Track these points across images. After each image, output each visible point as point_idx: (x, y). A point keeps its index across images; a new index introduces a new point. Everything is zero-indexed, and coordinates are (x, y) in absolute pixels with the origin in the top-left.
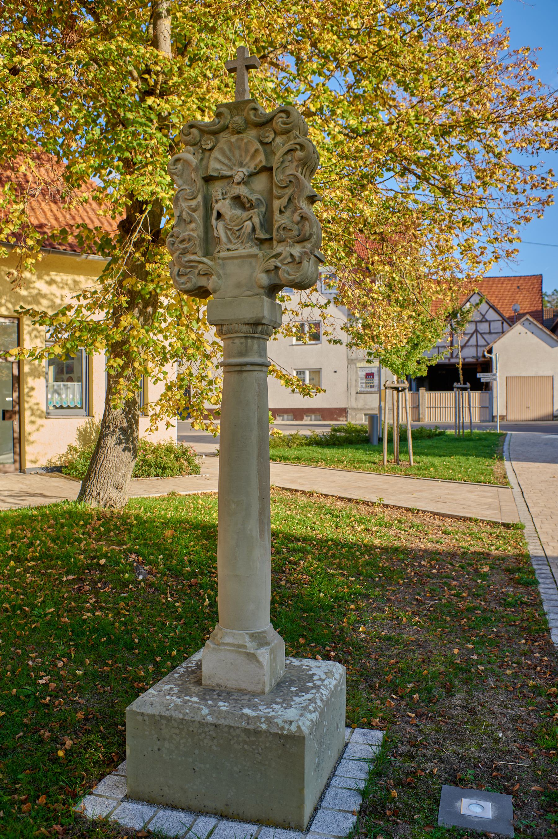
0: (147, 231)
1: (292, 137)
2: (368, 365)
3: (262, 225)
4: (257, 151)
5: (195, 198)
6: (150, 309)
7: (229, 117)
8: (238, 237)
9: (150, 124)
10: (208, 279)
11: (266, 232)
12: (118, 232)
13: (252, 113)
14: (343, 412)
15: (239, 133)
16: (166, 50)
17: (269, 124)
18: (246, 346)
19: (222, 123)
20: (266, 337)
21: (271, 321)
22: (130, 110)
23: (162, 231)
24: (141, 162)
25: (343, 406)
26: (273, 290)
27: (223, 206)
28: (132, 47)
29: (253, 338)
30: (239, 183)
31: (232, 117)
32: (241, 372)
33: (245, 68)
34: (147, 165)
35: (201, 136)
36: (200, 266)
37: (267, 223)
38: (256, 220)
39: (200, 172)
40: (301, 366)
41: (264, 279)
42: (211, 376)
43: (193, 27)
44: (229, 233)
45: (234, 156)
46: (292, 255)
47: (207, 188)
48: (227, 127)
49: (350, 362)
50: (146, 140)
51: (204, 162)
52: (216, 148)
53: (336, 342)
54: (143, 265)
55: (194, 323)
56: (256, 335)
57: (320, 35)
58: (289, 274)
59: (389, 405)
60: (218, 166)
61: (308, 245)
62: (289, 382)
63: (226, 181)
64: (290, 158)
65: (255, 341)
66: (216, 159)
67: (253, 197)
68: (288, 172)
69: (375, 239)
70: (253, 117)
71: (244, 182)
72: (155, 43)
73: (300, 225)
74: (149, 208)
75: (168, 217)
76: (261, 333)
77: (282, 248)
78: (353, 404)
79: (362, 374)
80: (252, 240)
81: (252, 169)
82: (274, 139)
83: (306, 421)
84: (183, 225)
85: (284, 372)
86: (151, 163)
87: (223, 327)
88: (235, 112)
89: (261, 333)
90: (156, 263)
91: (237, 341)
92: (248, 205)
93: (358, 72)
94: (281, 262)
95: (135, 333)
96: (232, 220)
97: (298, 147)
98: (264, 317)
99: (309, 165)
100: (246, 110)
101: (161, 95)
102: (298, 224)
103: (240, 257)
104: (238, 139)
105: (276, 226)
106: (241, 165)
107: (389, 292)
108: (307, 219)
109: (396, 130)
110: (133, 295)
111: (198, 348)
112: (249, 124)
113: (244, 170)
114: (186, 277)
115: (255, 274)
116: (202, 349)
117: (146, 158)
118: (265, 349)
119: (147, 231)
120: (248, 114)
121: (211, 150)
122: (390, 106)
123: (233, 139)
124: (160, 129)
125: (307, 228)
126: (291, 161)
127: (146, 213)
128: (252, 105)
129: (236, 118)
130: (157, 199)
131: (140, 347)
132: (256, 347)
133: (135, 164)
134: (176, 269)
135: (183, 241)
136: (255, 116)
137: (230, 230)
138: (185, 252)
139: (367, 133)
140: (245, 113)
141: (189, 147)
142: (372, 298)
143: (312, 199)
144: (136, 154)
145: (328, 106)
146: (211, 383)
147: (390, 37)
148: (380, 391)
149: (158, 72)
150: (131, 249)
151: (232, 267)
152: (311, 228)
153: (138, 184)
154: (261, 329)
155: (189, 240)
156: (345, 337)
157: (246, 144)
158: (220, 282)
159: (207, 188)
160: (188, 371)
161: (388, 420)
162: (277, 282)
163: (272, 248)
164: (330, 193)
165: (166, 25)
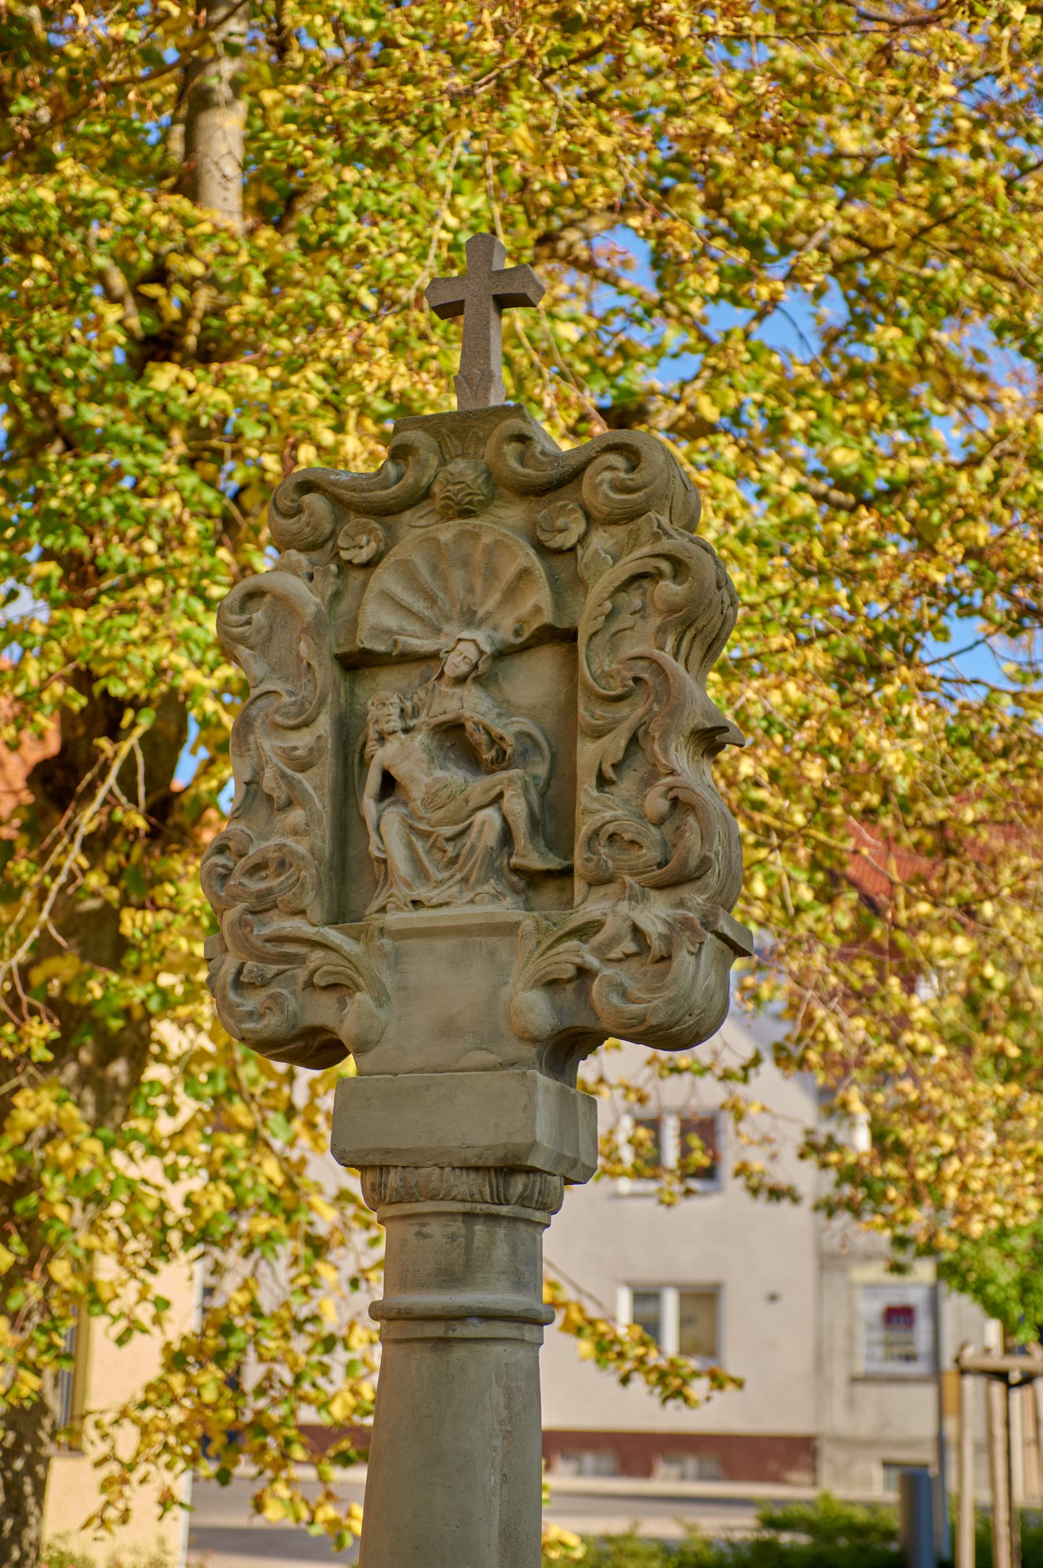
0: (133, 800)
1: (645, 535)
2: (894, 1278)
3: (535, 824)
4: (524, 573)
5: (306, 724)
6: (119, 1069)
7: (434, 462)
8: (453, 861)
9: (160, 445)
10: (342, 1004)
11: (551, 846)
12: (27, 798)
13: (511, 450)
14: (798, 1452)
15: (466, 513)
16: (224, 205)
17: (569, 488)
18: (468, 1248)
19: (409, 479)
20: (538, 1216)
21: (560, 1158)
22: (96, 396)
23: (186, 800)
24: (122, 568)
25: (799, 1425)
26: (568, 1047)
27: (406, 754)
28: (111, 194)
29: (495, 1218)
30: (460, 681)
31: (444, 462)
32: (446, 1341)
33: (491, 305)
34: (142, 578)
35: (339, 522)
36: (317, 956)
37: (554, 818)
38: (516, 806)
39: (330, 638)
40: (647, 1273)
41: (538, 1011)
42: (332, 1321)
43: (318, 153)
44: (419, 845)
45: (446, 589)
46: (636, 931)
47: (352, 693)
48: (427, 494)
49: (830, 1262)
50: (144, 495)
51: (345, 605)
52: (387, 562)
53: (776, 1194)
54: (109, 915)
55: (276, 1120)
56: (504, 1210)
57: (740, 173)
58: (625, 995)
59: (973, 1433)
60: (391, 620)
61: (696, 898)
62: (606, 1348)
63: (416, 671)
64: (637, 603)
65: (501, 1232)
66: (387, 596)
67: (508, 729)
68: (631, 648)
69: (918, 845)
70: (514, 464)
71: (478, 676)
72: (189, 185)
73: (668, 827)
74: (146, 721)
75: (204, 753)
76: (524, 1200)
77: (606, 905)
78: (838, 1420)
79: (872, 1308)
80: (498, 873)
81: (506, 634)
82: (582, 539)
83: (665, 1480)
84: (263, 812)
85: (593, 1312)
86: (160, 573)
87: (386, 1178)
88: (453, 444)
89: (524, 1200)
90: (158, 909)
91: (435, 1229)
92: (488, 755)
93: (862, 289)
94: (600, 951)
95: (64, 1152)
96: (431, 801)
97: (665, 566)
98: (533, 1145)
99: (702, 624)
100: (492, 442)
101: (204, 356)
102: (659, 823)
103: (459, 931)
104: (461, 535)
105: (584, 828)
106: (470, 618)
107: (969, 1026)
108: (691, 808)
109: (993, 489)
110: (72, 1017)
111: (289, 1215)
112: (498, 486)
113: (480, 636)
114: (264, 993)
115: (506, 991)
116: (302, 1217)
117: (142, 554)
118: (535, 1259)
119: (133, 800)
120: (499, 454)
121: (369, 565)
122: (969, 400)
123: (447, 532)
124: (191, 462)
125: (692, 839)
126: (641, 612)
127: (132, 741)
128: (513, 424)
129: (458, 466)
130: (173, 691)
131: (77, 1203)
132: (501, 1252)
133: (101, 573)
134: (229, 965)
135: (256, 869)
136: (522, 460)
137: (425, 835)
138: (263, 905)
139: (894, 491)
140: (488, 451)
141: (294, 554)
142: (912, 1048)
143: (710, 740)
144: (107, 543)
145: (760, 405)
146: (329, 1343)
147: (969, 182)
148: (937, 1375)
149: (194, 278)
150: (76, 858)
151: (427, 966)
152: (705, 837)
153: (111, 639)
154: (517, 1186)
155: (282, 864)
156: (810, 1180)
157: (490, 551)
158: (383, 1014)
159: (352, 693)
160: (243, 1298)
161: (969, 1488)
162: (583, 1020)
163: (569, 904)
164: (763, 693)
165: (226, 130)
